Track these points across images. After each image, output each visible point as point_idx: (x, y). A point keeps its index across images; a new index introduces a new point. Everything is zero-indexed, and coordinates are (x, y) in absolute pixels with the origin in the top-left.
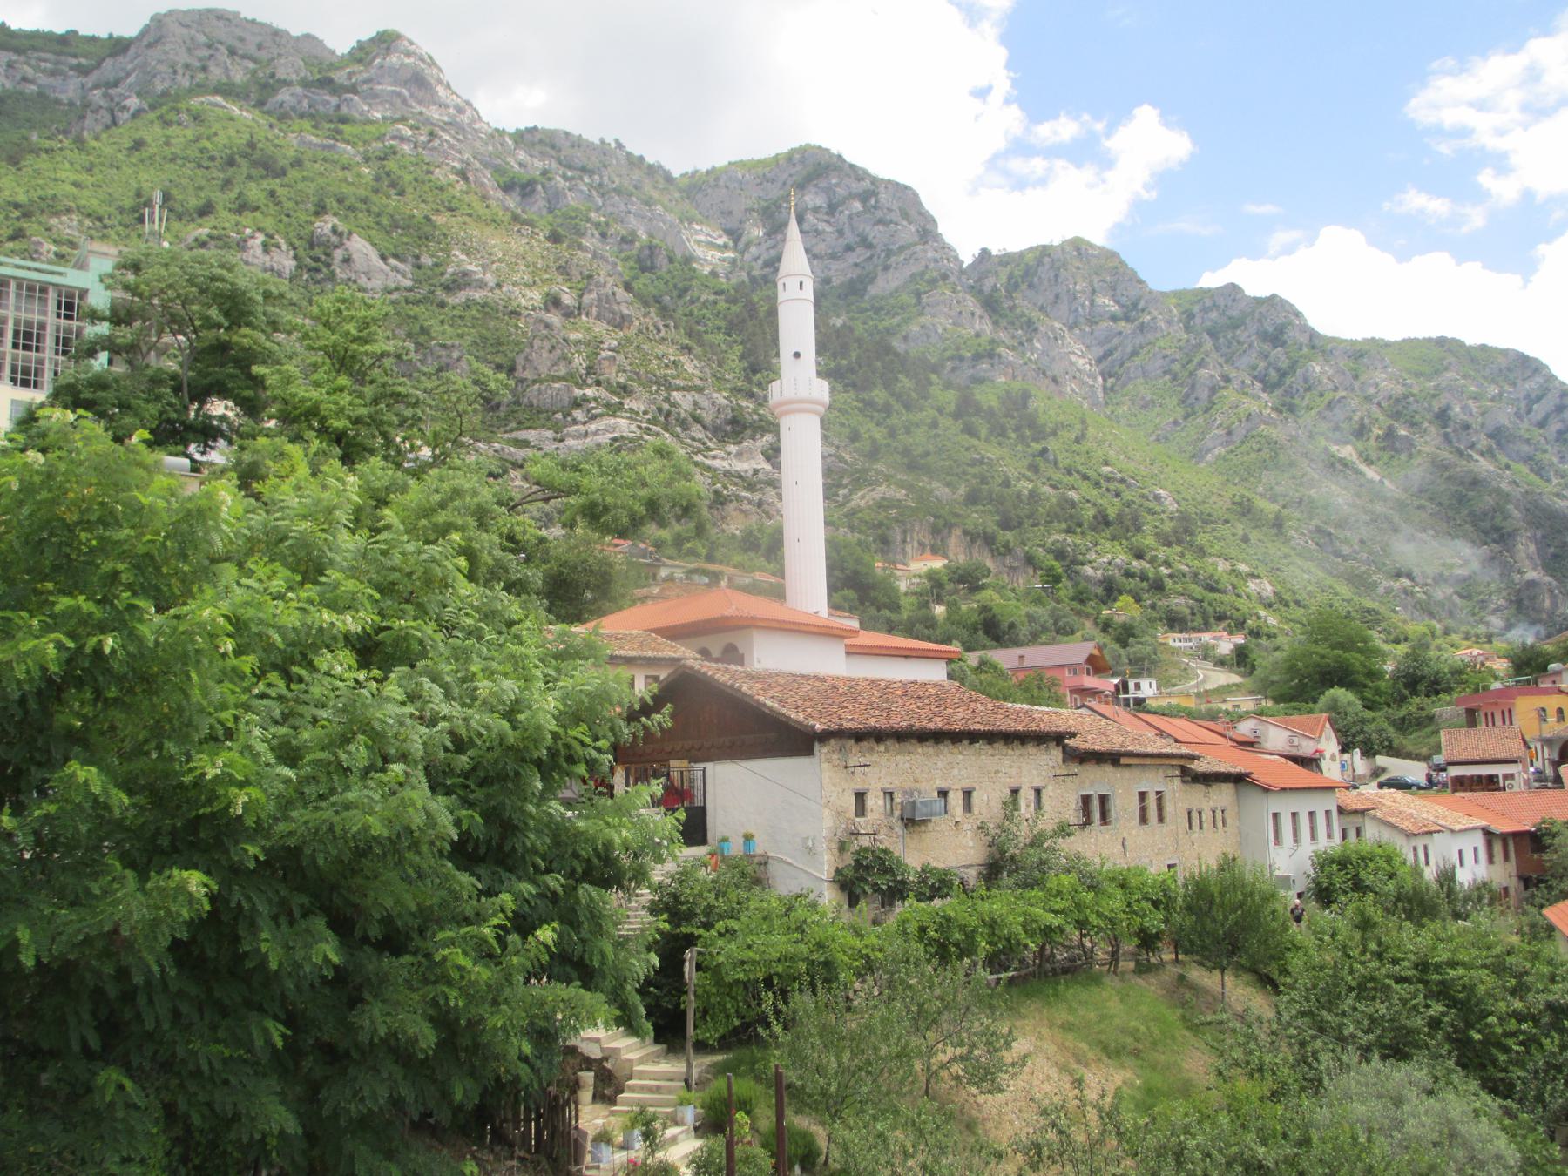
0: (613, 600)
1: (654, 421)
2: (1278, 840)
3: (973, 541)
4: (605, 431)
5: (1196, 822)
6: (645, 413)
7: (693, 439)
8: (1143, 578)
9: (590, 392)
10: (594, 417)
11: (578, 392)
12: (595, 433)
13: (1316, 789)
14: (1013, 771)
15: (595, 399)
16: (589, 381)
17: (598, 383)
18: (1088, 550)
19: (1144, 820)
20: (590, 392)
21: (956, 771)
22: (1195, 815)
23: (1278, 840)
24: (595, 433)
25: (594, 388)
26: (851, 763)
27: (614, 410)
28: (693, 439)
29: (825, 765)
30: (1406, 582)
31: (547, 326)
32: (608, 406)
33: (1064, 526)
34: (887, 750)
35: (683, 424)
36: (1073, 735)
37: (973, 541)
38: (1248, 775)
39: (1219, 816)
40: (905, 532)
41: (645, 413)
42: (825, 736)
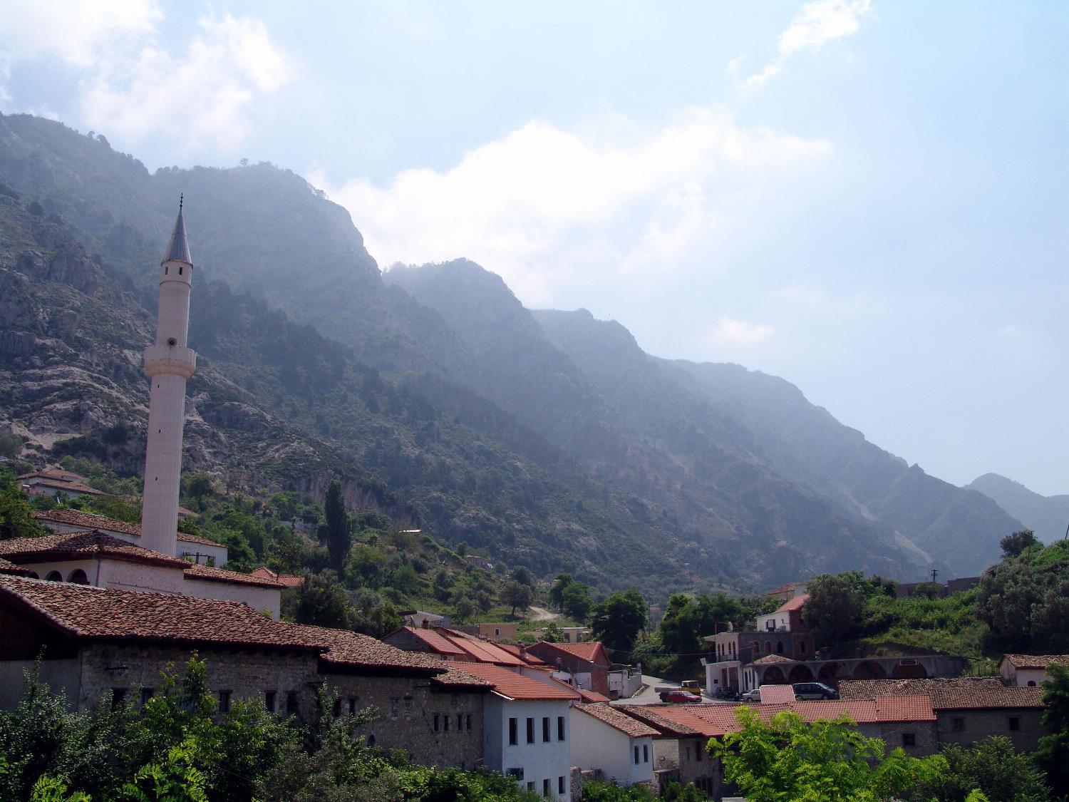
0: (367, 559)
1: (106, 373)
2: (513, 740)
3: (365, 492)
4: (59, 377)
5: (442, 724)
6: (98, 365)
7: (138, 391)
8: (499, 531)
9: (48, 342)
10: (50, 365)
11: (39, 341)
12: (50, 378)
13: (538, 699)
14: (271, 678)
15: (53, 349)
16: (50, 333)
17: (58, 336)
18: (458, 506)
19: (637, 761)
20: (48, 342)
21: (215, 677)
22: (441, 719)
23: (513, 740)
24: (50, 378)
25: (54, 340)
26: (113, 665)
27: (71, 359)
28: (138, 391)
29: (86, 667)
30: (694, 544)
31: (17, 282)
32: (65, 356)
33: (440, 486)
34: (149, 656)
35: (132, 379)
36: (326, 650)
37: (365, 492)
38: (493, 687)
39: (464, 721)
40: (309, 481)
41: (98, 365)
42: (89, 641)
